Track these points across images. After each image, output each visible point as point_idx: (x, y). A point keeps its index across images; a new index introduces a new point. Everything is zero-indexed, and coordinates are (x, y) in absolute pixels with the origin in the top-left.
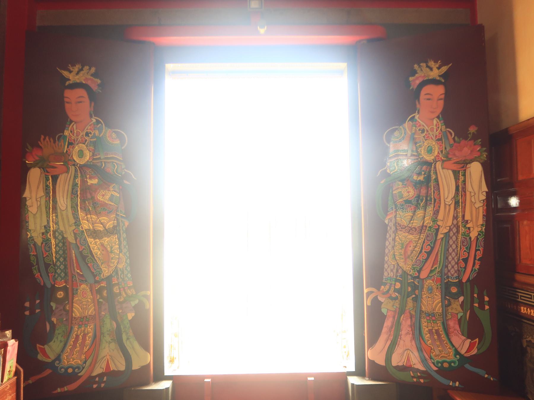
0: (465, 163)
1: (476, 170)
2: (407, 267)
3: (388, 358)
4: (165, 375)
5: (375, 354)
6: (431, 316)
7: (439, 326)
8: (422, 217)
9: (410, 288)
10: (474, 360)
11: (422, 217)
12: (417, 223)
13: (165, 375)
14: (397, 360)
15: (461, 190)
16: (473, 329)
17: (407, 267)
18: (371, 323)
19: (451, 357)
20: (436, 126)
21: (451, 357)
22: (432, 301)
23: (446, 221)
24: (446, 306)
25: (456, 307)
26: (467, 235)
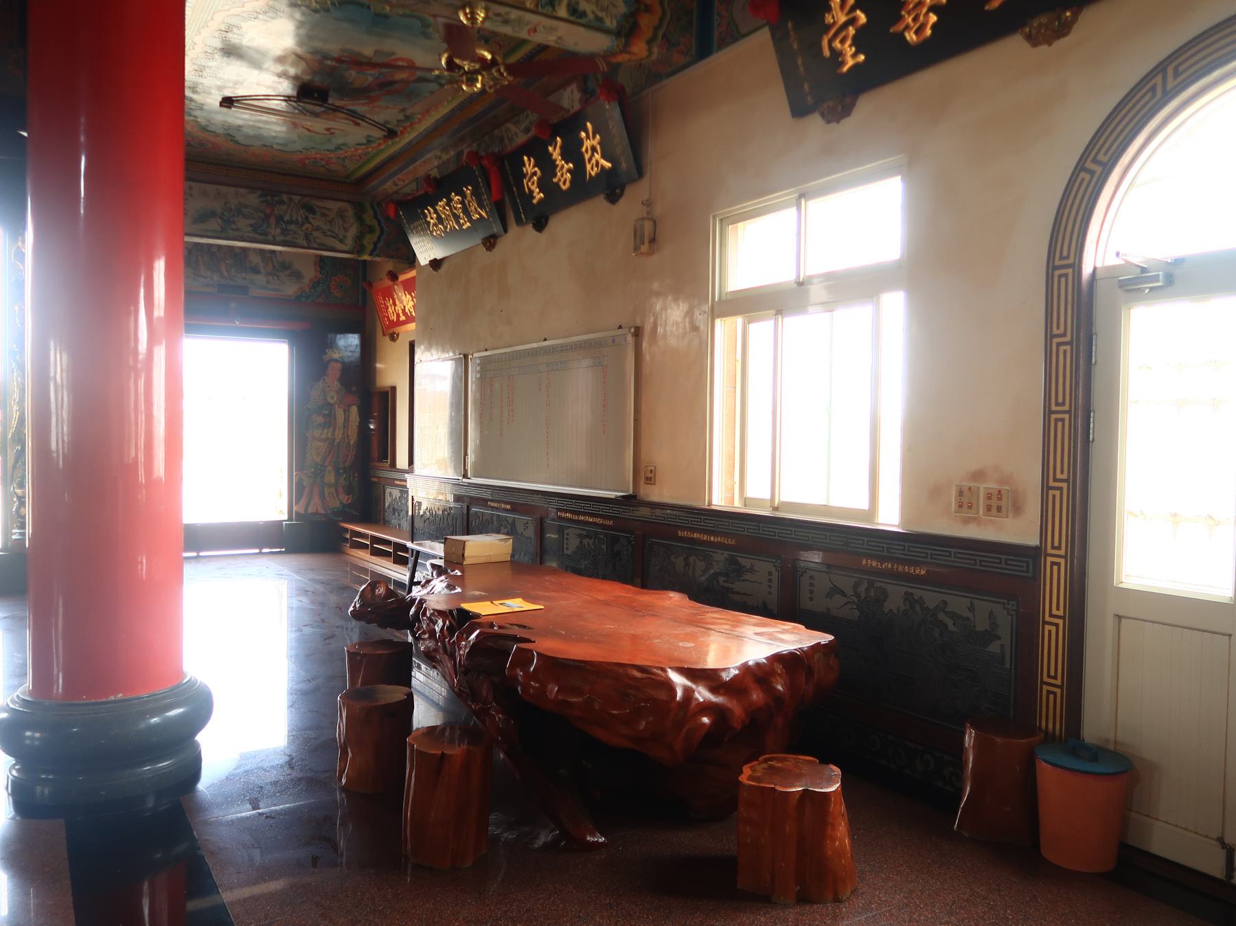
0: (349, 406)
1: (354, 409)
2: (318, 460)
3: (306, 510)
4: (899, 178)
5: (318, 44)
6: (329, 485)
7: (333, 490)
8: (327, 433)
9: (319, 471)
10: (349, 506)
11: (327, 433)
12: (324, 436)
13: (899, 178)
14: (310, 510)
15: (347, 420)
16: (349, 490)
17: (318, 460)
18: (298, 490)
19: (338, 504)
20: (337, 385)
21: (338, 504)
22: (330, 477)
23: (339, 435)
24: (337, 480)
25: (342, 480)
26: (348, 443)
